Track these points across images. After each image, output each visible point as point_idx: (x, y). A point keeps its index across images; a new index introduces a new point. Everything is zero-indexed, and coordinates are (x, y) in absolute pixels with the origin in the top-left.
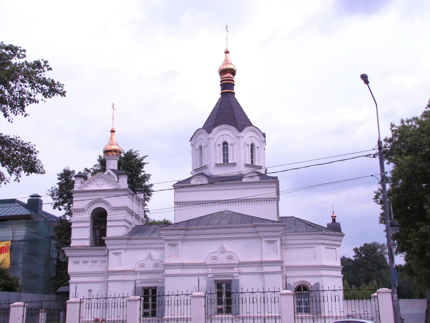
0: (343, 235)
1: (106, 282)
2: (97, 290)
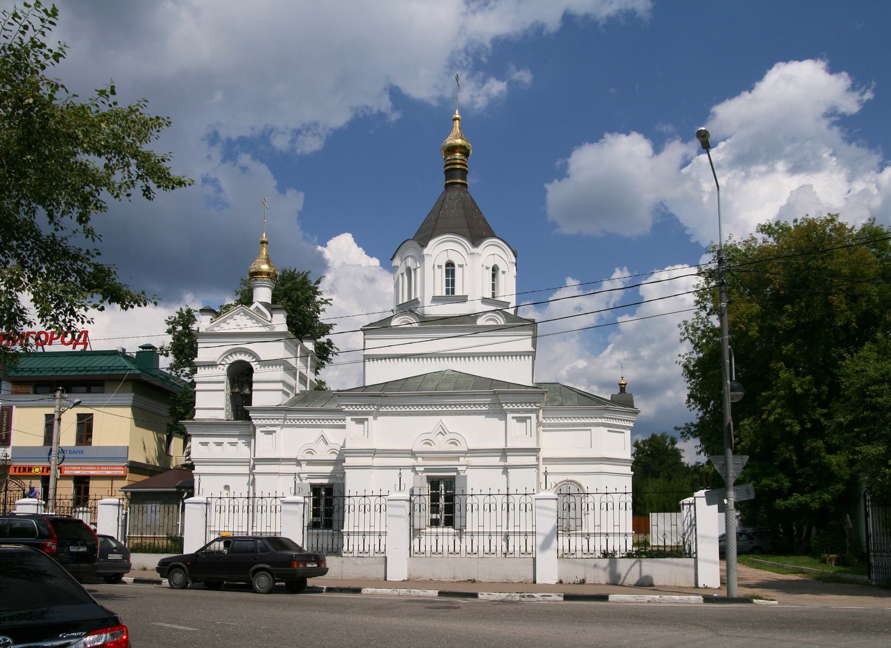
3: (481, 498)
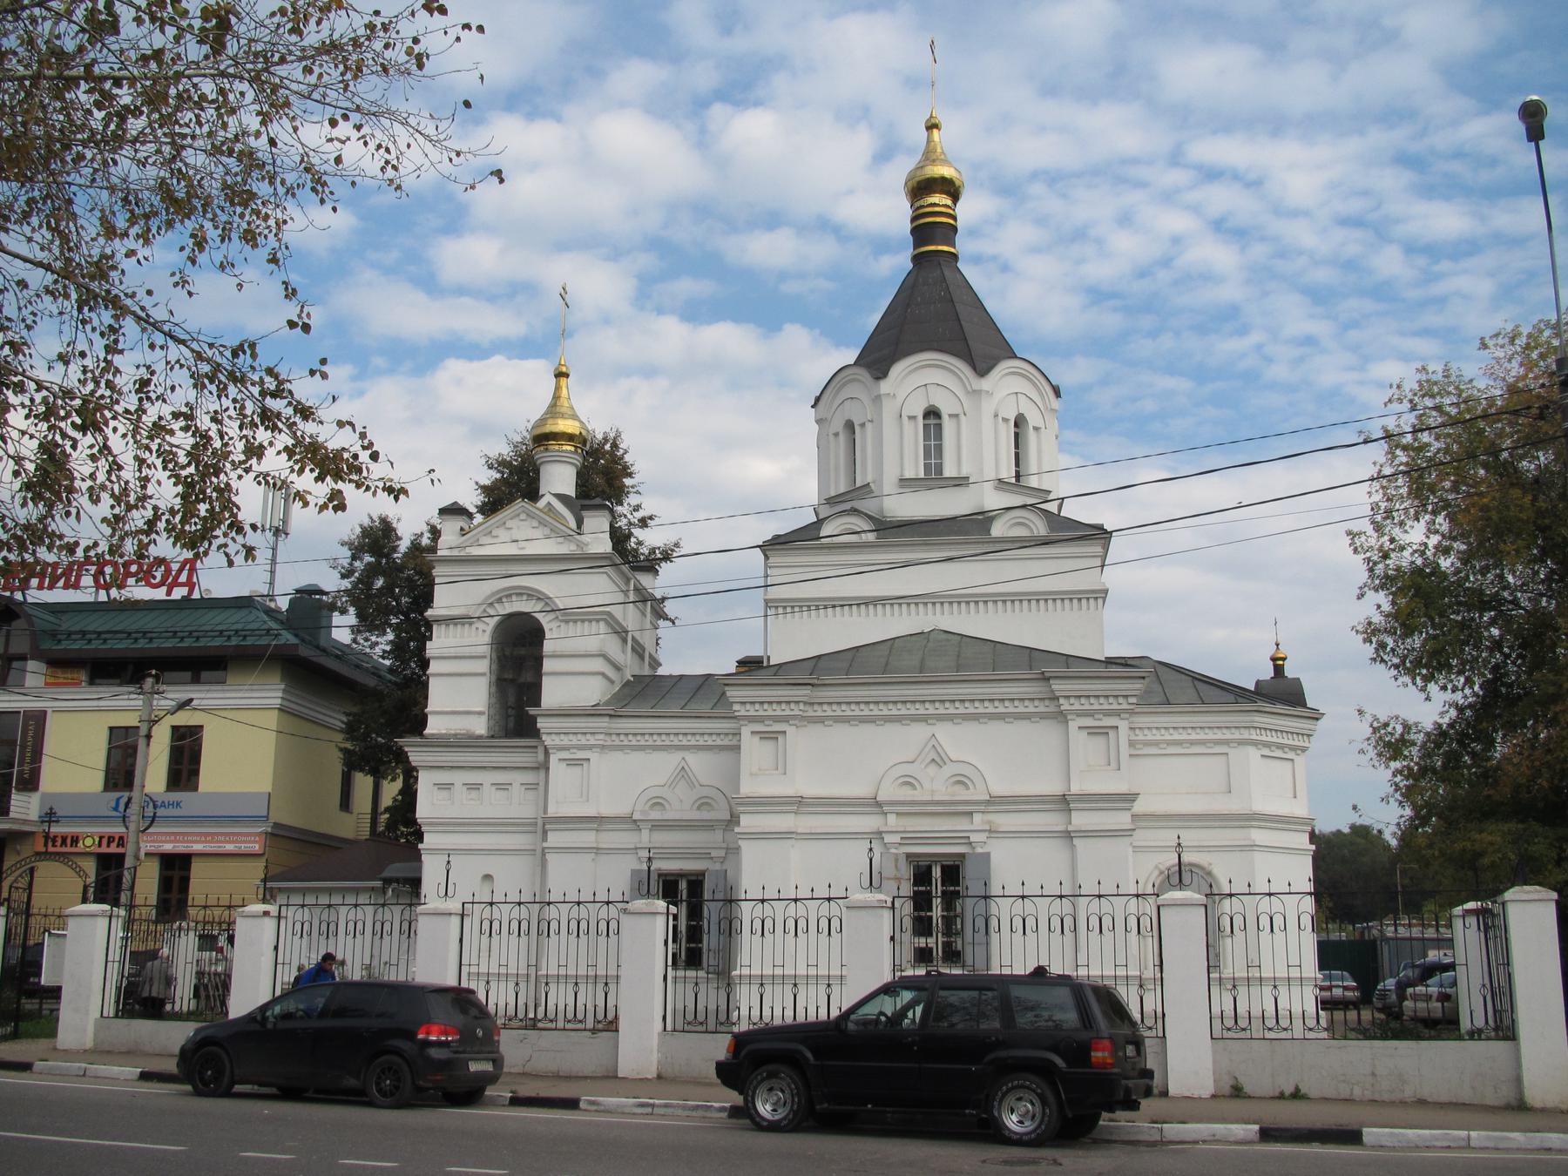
0: (1316, 716)
1: (539, 851)
2: (512, 878)
3: (564, 908)
